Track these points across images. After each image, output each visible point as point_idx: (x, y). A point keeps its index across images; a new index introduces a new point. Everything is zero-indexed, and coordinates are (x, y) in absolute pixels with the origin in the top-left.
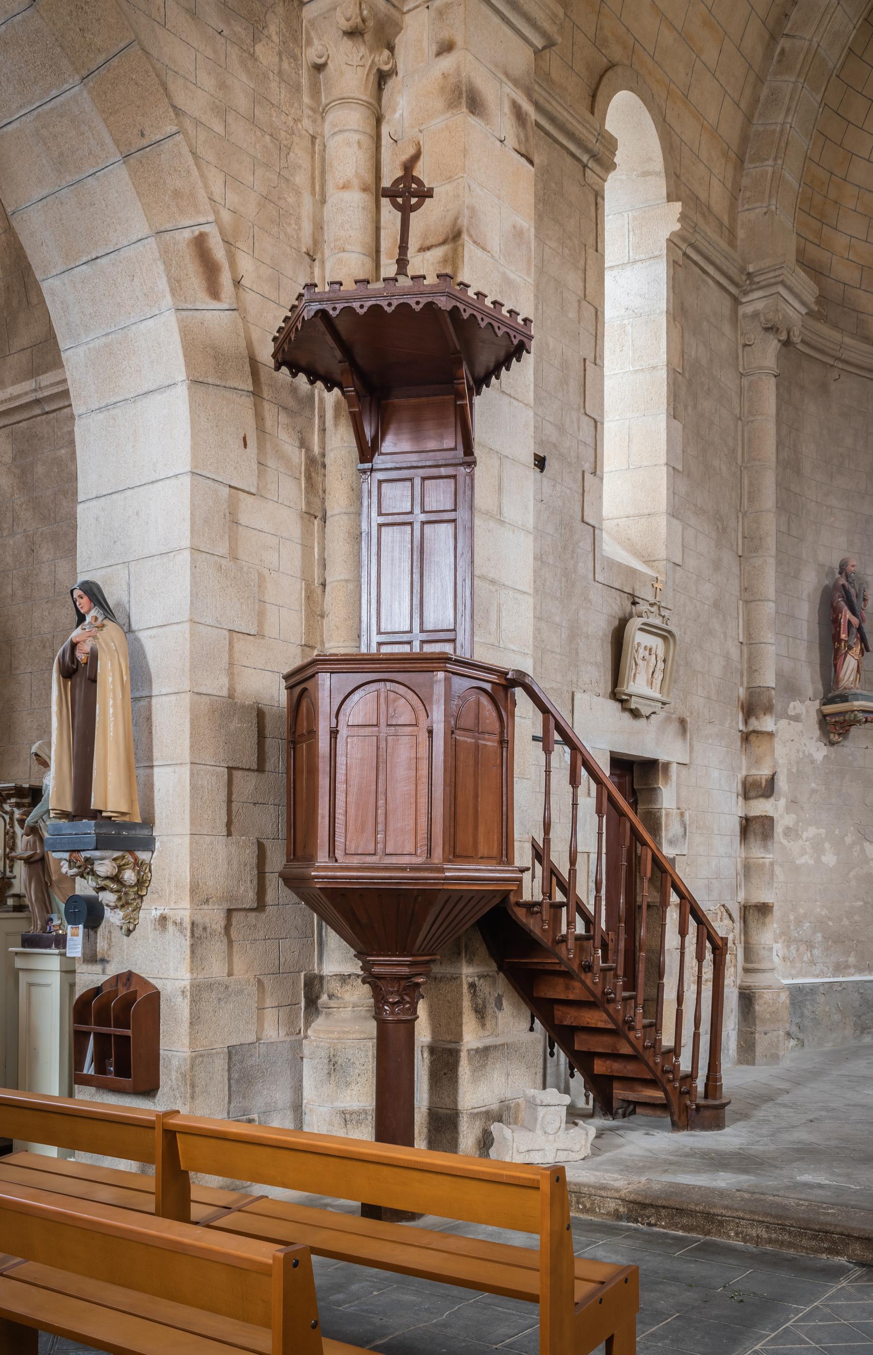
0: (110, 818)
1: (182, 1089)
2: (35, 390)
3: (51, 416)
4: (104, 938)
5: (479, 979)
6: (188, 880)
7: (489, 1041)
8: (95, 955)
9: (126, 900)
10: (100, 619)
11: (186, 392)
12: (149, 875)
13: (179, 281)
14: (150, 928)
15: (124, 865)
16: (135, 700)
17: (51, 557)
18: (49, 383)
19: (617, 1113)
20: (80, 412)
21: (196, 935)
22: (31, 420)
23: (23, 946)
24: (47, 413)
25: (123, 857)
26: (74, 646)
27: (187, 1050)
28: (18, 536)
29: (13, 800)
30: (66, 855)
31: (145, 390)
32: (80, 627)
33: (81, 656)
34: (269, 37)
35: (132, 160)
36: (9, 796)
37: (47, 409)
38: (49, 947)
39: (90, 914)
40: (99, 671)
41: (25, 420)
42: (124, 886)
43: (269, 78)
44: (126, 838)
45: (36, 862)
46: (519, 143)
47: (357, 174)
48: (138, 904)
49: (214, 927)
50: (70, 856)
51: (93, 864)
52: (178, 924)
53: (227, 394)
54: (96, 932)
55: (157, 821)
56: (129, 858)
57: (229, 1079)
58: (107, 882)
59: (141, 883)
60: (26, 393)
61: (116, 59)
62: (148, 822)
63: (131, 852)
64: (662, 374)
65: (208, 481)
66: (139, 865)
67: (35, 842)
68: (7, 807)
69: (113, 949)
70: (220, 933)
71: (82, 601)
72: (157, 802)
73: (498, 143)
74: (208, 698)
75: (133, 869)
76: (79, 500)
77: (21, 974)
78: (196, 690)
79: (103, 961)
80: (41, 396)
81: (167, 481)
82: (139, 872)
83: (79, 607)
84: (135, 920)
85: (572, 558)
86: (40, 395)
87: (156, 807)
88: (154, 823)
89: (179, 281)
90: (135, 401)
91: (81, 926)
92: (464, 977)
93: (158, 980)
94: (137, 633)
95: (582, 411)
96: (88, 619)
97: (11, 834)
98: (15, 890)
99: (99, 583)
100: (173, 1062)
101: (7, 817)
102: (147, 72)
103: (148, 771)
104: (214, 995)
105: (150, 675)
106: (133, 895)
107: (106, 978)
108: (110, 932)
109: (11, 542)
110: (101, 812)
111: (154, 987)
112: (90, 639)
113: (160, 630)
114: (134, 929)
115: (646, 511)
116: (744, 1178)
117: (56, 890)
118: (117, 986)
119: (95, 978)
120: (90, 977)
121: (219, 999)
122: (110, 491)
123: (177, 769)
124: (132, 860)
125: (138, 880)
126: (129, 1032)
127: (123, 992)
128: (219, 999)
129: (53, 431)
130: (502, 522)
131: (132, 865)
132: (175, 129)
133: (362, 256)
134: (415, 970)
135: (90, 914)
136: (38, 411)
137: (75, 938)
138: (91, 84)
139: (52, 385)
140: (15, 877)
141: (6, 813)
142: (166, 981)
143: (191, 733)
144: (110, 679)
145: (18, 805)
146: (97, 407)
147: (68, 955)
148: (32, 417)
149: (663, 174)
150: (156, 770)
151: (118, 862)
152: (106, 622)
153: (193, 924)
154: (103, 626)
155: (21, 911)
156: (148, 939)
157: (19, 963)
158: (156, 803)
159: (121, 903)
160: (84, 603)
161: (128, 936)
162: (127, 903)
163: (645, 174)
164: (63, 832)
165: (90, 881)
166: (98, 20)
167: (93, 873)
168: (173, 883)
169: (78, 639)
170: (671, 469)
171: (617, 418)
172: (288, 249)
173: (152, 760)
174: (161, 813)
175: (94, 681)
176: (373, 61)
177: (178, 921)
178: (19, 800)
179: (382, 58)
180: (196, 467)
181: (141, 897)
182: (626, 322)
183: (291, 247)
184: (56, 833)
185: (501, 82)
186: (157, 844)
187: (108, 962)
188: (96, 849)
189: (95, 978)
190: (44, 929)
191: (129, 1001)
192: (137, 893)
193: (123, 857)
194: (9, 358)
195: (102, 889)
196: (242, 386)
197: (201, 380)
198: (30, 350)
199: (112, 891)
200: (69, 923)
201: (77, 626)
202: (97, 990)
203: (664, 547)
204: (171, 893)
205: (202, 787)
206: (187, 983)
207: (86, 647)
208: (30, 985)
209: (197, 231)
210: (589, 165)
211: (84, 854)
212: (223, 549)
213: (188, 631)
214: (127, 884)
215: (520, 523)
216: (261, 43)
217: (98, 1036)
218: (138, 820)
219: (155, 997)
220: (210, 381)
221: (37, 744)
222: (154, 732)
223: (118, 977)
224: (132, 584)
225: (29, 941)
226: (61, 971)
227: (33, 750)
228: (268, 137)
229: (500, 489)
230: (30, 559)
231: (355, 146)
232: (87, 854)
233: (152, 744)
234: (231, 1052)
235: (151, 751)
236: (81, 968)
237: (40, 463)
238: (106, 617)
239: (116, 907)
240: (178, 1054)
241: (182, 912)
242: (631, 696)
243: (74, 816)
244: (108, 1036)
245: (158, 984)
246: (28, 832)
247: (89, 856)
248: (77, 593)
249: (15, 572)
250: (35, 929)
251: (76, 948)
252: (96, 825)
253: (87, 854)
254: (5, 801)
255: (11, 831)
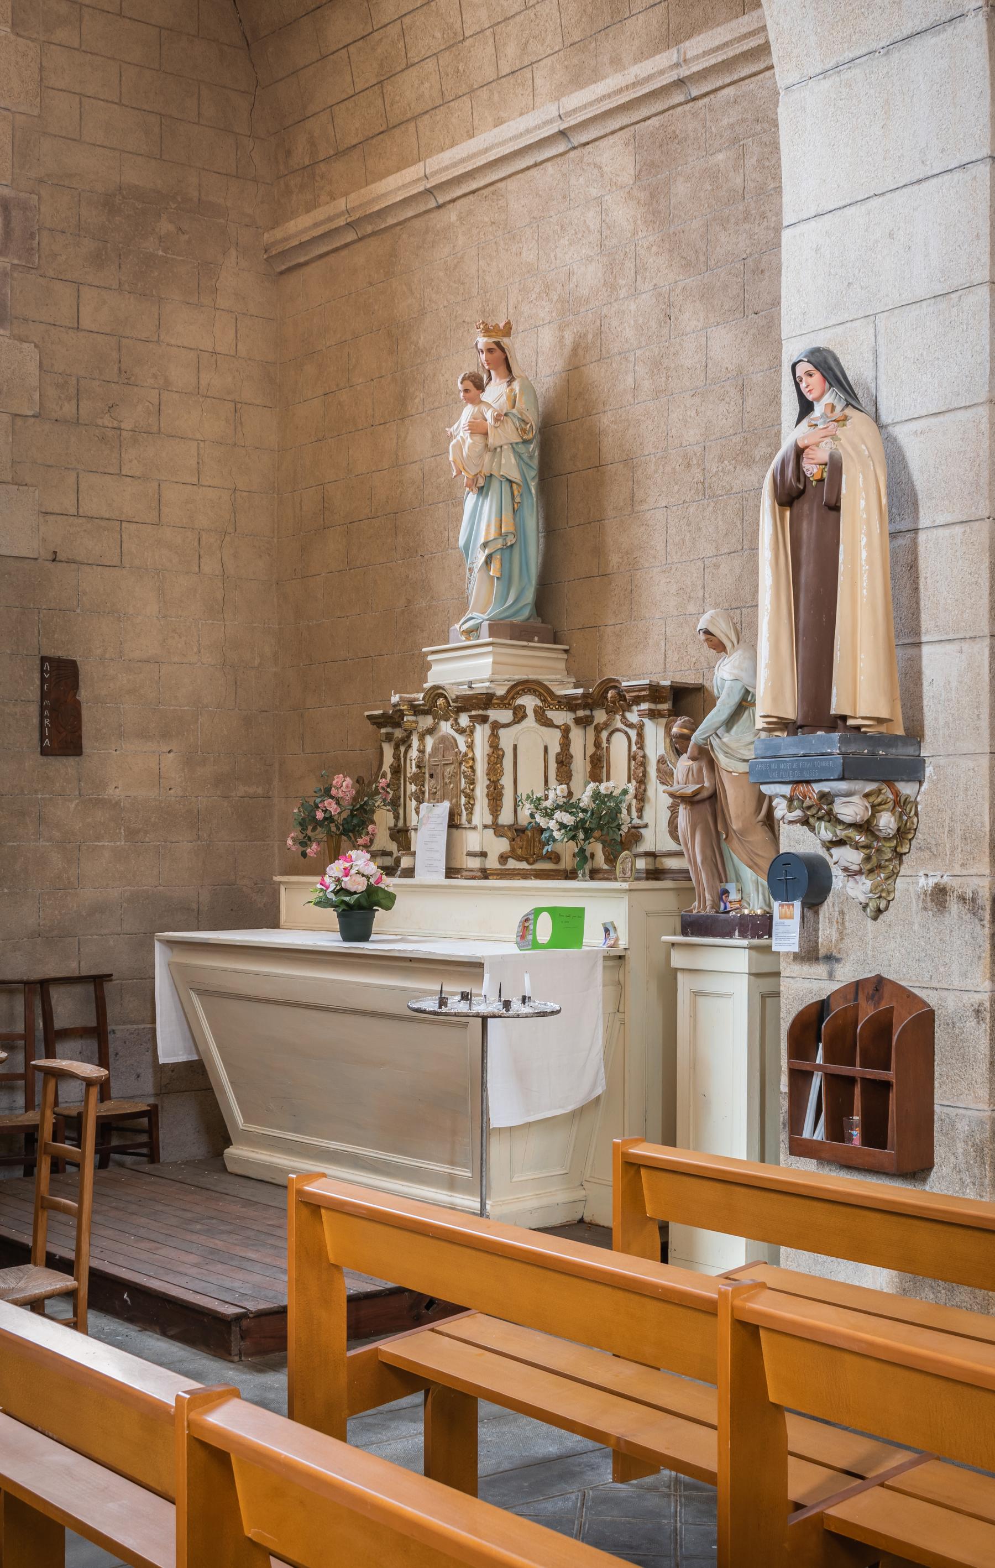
0: (858, 728)
1: (976, 1171)
2: (677, 65)
3: (700, 103)
4: (831, 922)
6: (987, 829)
8: (816, 948)
9: (879, 860)
10: (839, 408)
11: (983, 27)
12: (915, 820)
14: (915, 906)
15: (880, 804)
16: (894, 535)
17: (700, 325)
18: (700, 51)
20: (789, 81)
22: (666, 114)
23: (684, 933)
24: (694, 99)
25: (879, 791)
26: (799, 453)
27: (986, 1107)
28: (644, 296)
29: (645, 706)
30: (786, 790)
31: (906, 32)
32: (805, 422)
33: (811, 469)
36: (637, 701)
37: (695, 93)
38: (730, 934)
39: (805, 883)
40: (844, 491)
41: (655, 115)
42: (877, 838)
44: (884, 760)
45: (703, 801)
48: (895, 867)
50: (793, 790)
51: (832, 803)
52: (969, 902)
54: (817, 913)
55: (928, 733)
58: (851, 833)
59: (903, 833)
60: (662, 72)
62: (915, 734)
63: (889, 782)
66: (902, 805)
67: (700, 770)
68: (633, 717)
69: (847, 941)
71: (810, 380)
72: (927, 702)
75: (893, 811)
76: (785, 223)
77: (680, 976)
79: (829, 958)
80: (688, 73)
81: (947, 177)
82: (900, 817)
83: (805, 391)
84: (889, 893)
86: (684, 72)
87: (926, 709)
88: (922, 736)
90: (887, 53)
91: (797, 904)
93: (930, 992)
94: (890, 428)
96: (819, 410)
97: (639, 759)
98: (647, 845)
99: (831, 348)
100: (959, 1125)
101: (633, 733)
103: (911, 651)
105: (916, 495)
106: (885, 851)
107: (835, 986)
108: (842, 913)
109: (633, 307)
110: (844, 718)
111: (925, 1004)
112: (828, 440)
113: (933, 420)
114: (887, 908)
117: (735, 843)
118: (856, 999)
119: (815, 985)
120: (807, 984)
122: (841, 204)
123: (966, 646)
124: (891, 796)
125: (899, 829)
126: (890, 1075)
127: (867, 1012)
129: (704, 126)
131: (891, 805)
135: (805, 883)
136: (678, 98)
137: (787, 922)
139: (705, 53)
140: (646, 826)
141: (631, 726)
142: (946, 993)
144: (863, 503)
145: (653, 715)
146: (818, 71)
147: (774, 949)
148: (668, 109)
150: (926, 649)
151: (871, 799)
152: (849, 412)
154: (846, 418)
155: (657, 879)
156: (912, 924)
157: (678, 959)
158: (925, 703)
159: (869, 867)
160: (813, 384)
161: (875, 919)
162: (879, 867)
164: (782, 753)
165: (823, 831)
167: (832, 818)
168: (958, 833)
169: (806, 442)
173: (918, 634)
174: (936, 719)
175: (836, 508)
177: (969, 895)
178: (653, 706)
181: (900, 856)
184: (769, 754)
186: (929, 771)
187: (838, 960)
188: (842, 778)
189: (815, 985)
190: (715, 906)
191: (882, 1026)
192: (895, 850)
193: (879, 791)
194: (629, 21)
195: (841, 843)
198: (358, 89)
199: (857, 846)
200: (775, 900)
201: (798, 422)
202: (822, 1007)
204: (954, 849)
206: (985, 998)
207: (822, 454)
208: (696, 994)
211: (817, 787)
213: (985, 420)
214: (882, 835)
217: (830, 1078)
218: (900, 731)
219: (925, 1020)
221: (707, 616)
222: (921, 587)
223: (858, 985)
224: (882, 350)
225: (695, 926)
226: (750, 974)
227: (702, 625)
230: (665, 331)
232: (825, 787)
233: (918, 608)
235: (918, 619)
236: (788, 969)
237: (681, 179)
238: (847, 405)
239: (860, 872)
240: (969, 1113)
241: (976, 881)
243: (801, 727)
244: (851, 1081)
245: (931, 998)
246: (696, 754)
247: (827, 790)
248: (802, 369)
249: (639, 352)
250: (702, 906)
251: (788, 938)
252: (843, 741)
253: (825, 787)
254: (628, 708)
255: (641, 753)
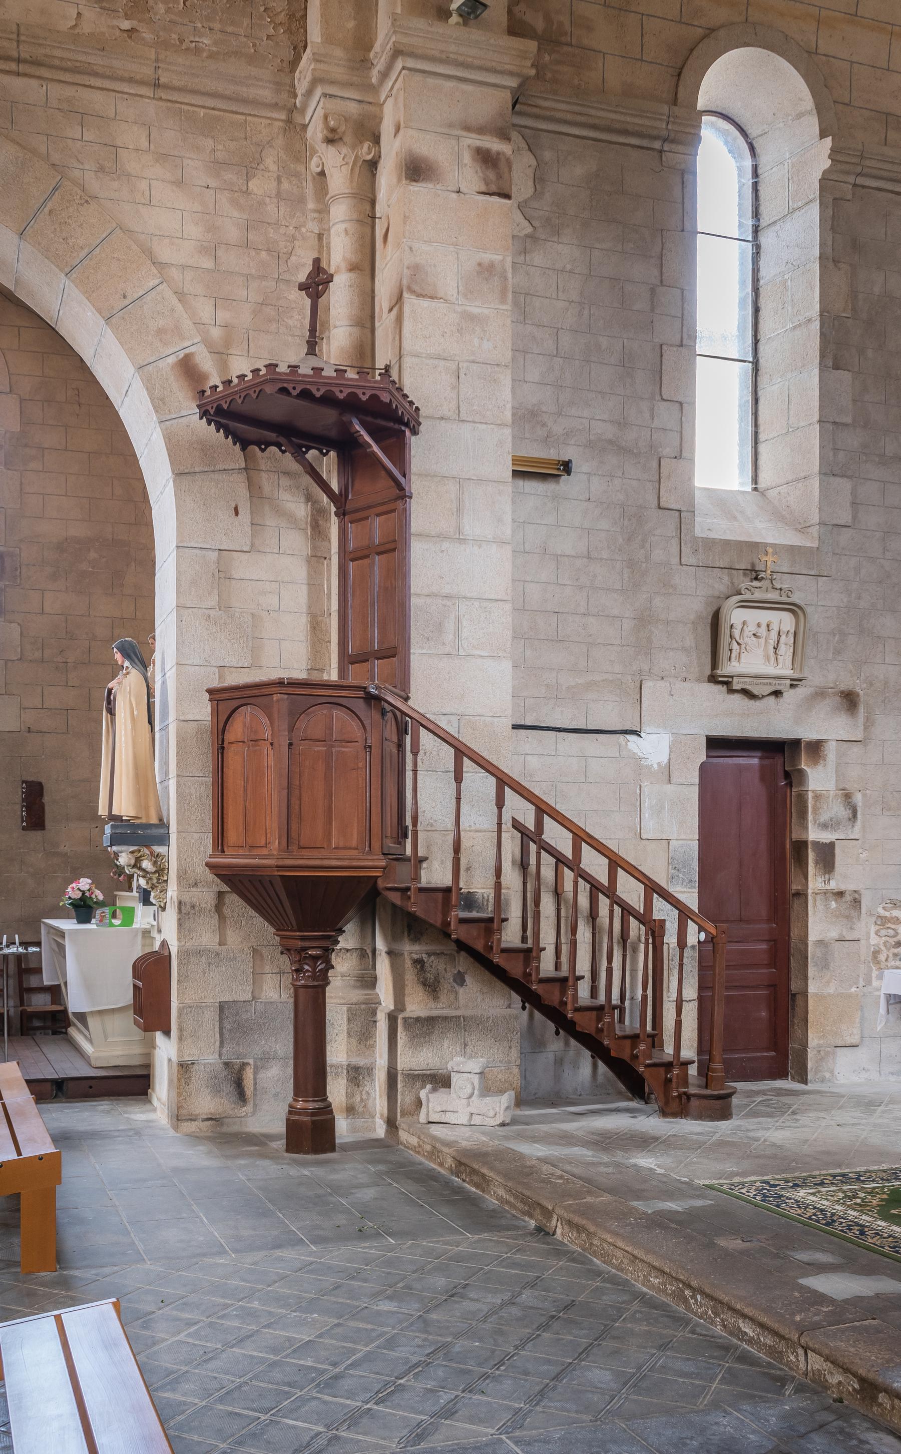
5: (429, 956)
7: (435, 1013)
13: (162, 400)
19: (649, 1098)
21: (184, 912)
34: (266, 170)
35: (114, 320)
43: (265, 204)
46: (487, 184)
47: (344, 259)
49: (203, 905)
53: (216, 476)
56: (146, 851)
57: (221, 1029)
61: (98, 249)
63: (147, 846)
64: (816, 325)
65: (195, 550)
66: (156, 858)
70: (210, 911)
73: (454, 195)
74: (196, 723)
78: (182, 718)
85: (642, 547)
89: (162, 400)
92: (406, 954)
95: (658, 397)
102: (129, 248)
104: (203, 960)
115: (802, 475)
116: (511, 1146)
121: (210, 963)
128: (210, 963)
130: (462, 541)
132: (157, 281)
133: (349, 328)
134: (307, 944)
138: (74, 276)
143: (177, 753)
149: (815, 112)
153: (180, 903)
163: (800, 116)
166: (81, 226)
170: (830, 427)
171: (779, 380)
172: (290, 338)
176: (356, 156)
179: (366, 152)
180: (181, 541)
182: (786, 277)
183: (293, 336)
185: (458, 138)
196: (233, 466)
197: (186, 471)
203: (817, 511)
205: (190, 794)
209: (181, 355)
210: (666, 148)
212: (213, 601)
215: (490, 536)
216: (256, 178)
218: (154, 821)
220: (197, 470)
228: (264, 253)
229: (458, 510)
231: (343, 235)
234: (222, 1007)
242: (732, 677)
